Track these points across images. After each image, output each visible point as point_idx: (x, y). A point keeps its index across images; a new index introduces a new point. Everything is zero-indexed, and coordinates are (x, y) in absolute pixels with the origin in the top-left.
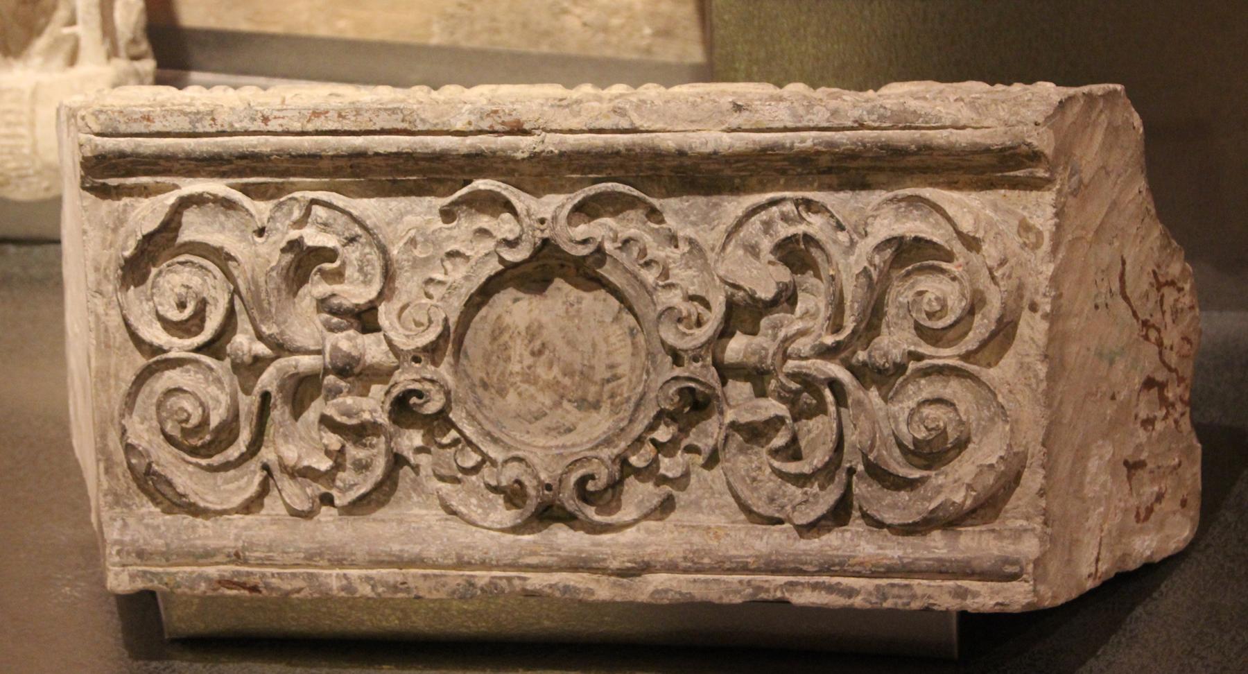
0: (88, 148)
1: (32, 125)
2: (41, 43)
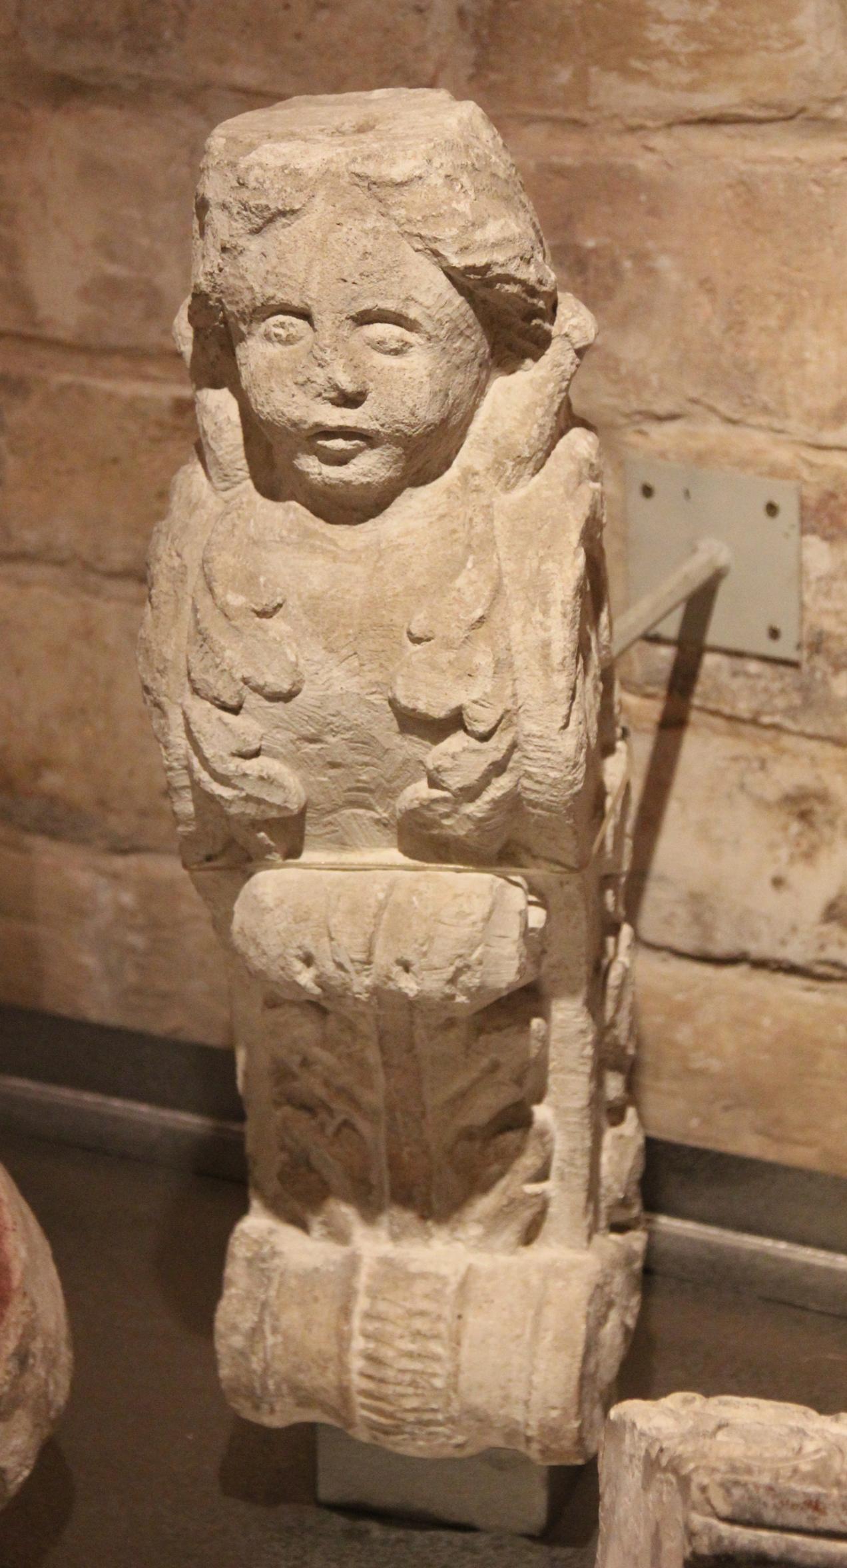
0: (705, 1540)
1: (456, 1341)
2: (486, 1204)
